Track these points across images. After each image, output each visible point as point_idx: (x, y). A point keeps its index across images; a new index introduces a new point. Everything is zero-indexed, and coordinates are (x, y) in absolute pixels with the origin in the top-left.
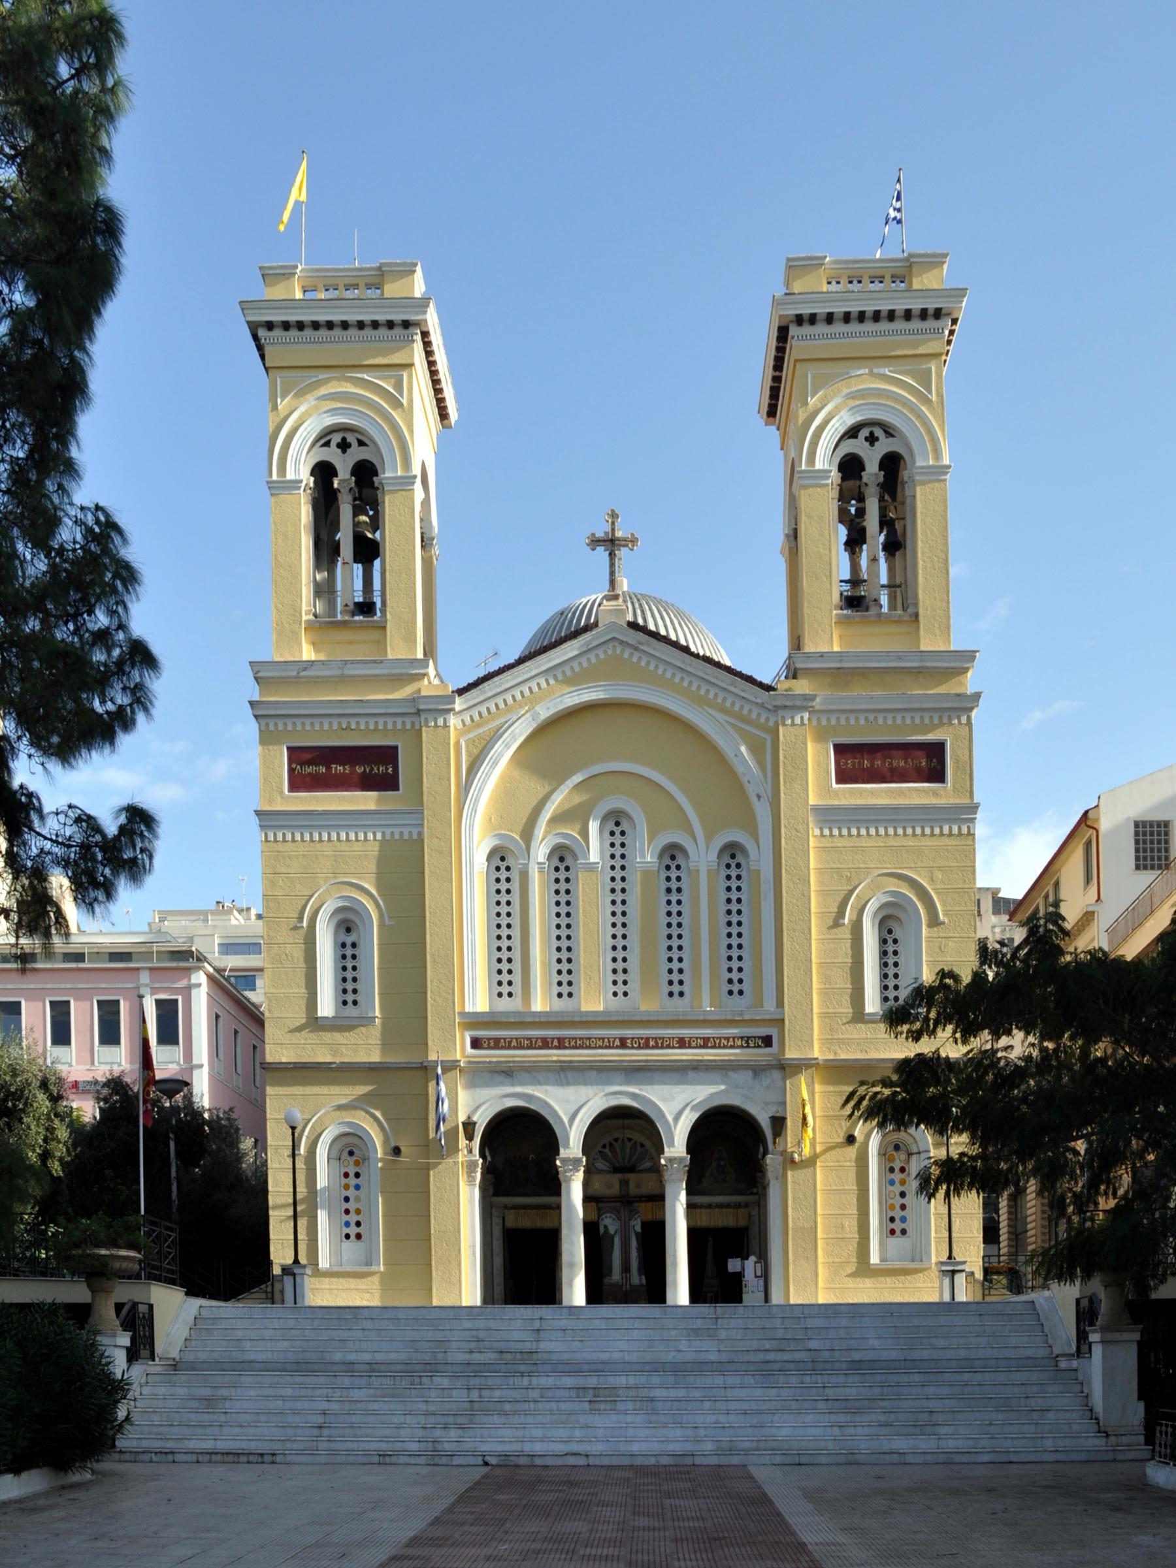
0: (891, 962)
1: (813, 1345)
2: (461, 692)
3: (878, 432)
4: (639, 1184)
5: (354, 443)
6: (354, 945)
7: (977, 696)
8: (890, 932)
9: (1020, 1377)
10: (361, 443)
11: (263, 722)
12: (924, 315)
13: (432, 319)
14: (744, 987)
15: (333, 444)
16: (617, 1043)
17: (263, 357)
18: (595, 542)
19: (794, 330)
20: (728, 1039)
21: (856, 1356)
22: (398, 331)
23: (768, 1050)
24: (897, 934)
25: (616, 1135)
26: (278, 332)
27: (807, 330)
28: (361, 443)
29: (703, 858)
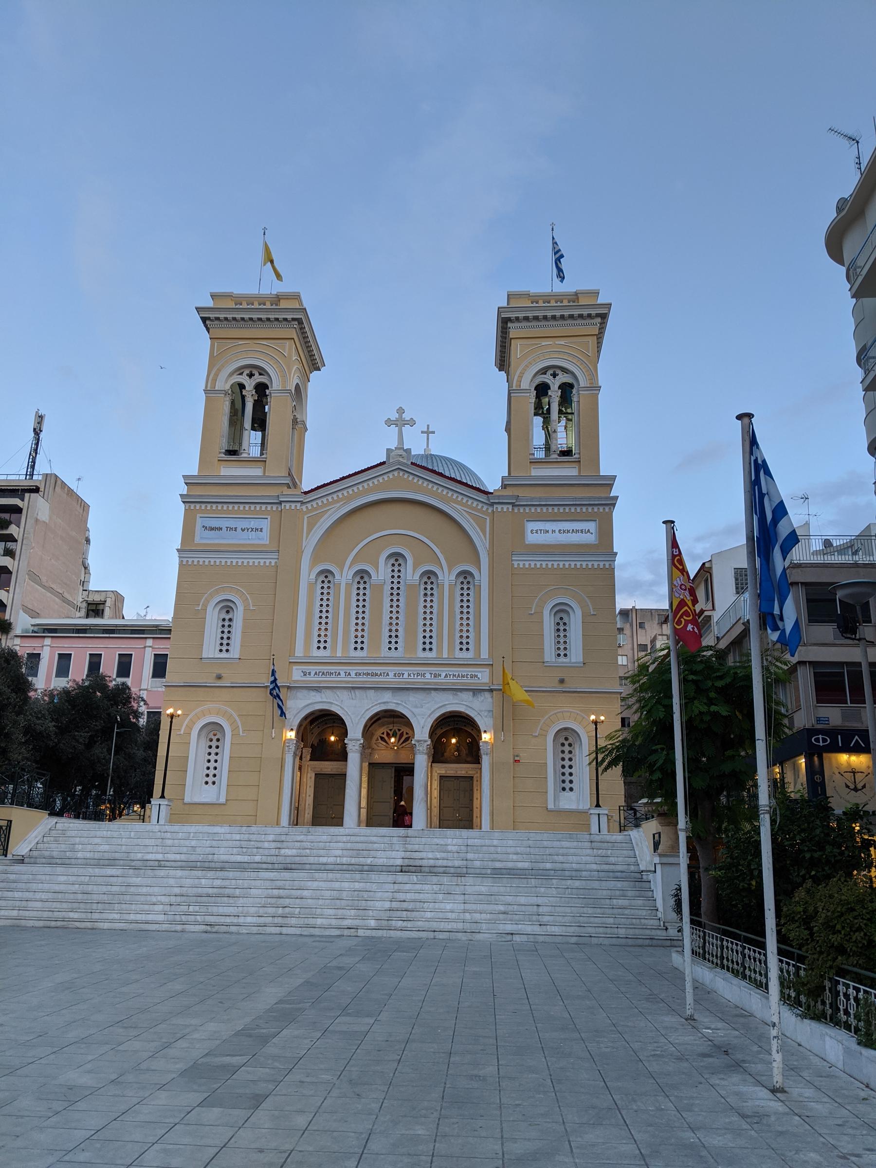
1: (470, 856)
3: (558, 371)
6: (230, 620)
8: (561, 619)
9: (611, 884)
11: (188, 505)
14: (470, 647)
15: (245, 374)
18: (389, 422)
21: (498, 865)
24: (566, 620)
28: (260, 374)
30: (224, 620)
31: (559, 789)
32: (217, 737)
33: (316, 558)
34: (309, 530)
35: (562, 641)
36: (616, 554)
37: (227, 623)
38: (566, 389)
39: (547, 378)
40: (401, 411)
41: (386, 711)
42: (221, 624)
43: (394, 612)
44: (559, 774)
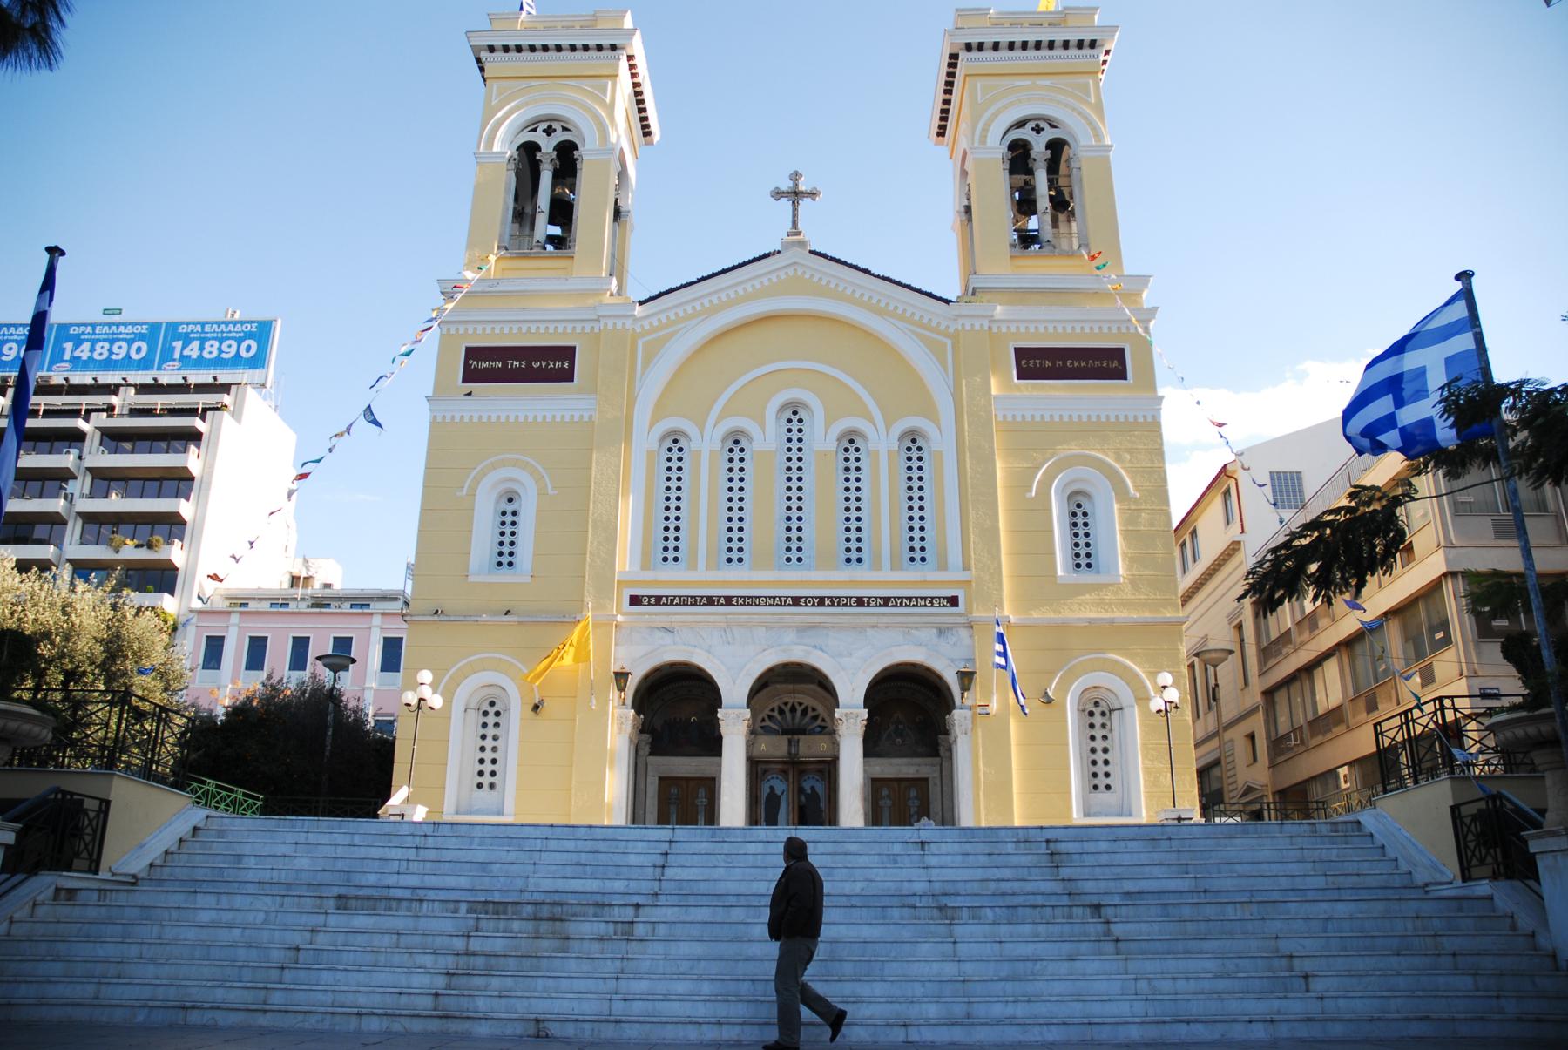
0: (1081, 533)
2: (641, 303)
4: (810, 747)
5: (559, 129)
6: (515, 513)
7: (1155, 309)
8: (1079, 506)
10: (565, 129)
12: (1080, 44)
13: (637, 46)
15: (540, 130)
16: (789, 601)
17: (482, 69)
18: (778, 194)
19: (963, 55)
20: (910, 598)
22: (606, 53)
23: (954, 610)
24: (1086, 507)
25: (786, 700)
26: (499, 54)
27: (975, 54)
28: (565, 129)
29: (882, 444)
30: (504, 513)
31: (1089, 787)
32: (495, 709)
33: (659, 412)
34: (648, 361)
35: (1081, 533)
36: (1162, 398)
37: (509, 519)
38: (1056, 147)
39: (1026, 133)
40: (795, 177)
41: (786, 666)
42: (500, 520)
43: (794, 498)
44: (1087, 762)
